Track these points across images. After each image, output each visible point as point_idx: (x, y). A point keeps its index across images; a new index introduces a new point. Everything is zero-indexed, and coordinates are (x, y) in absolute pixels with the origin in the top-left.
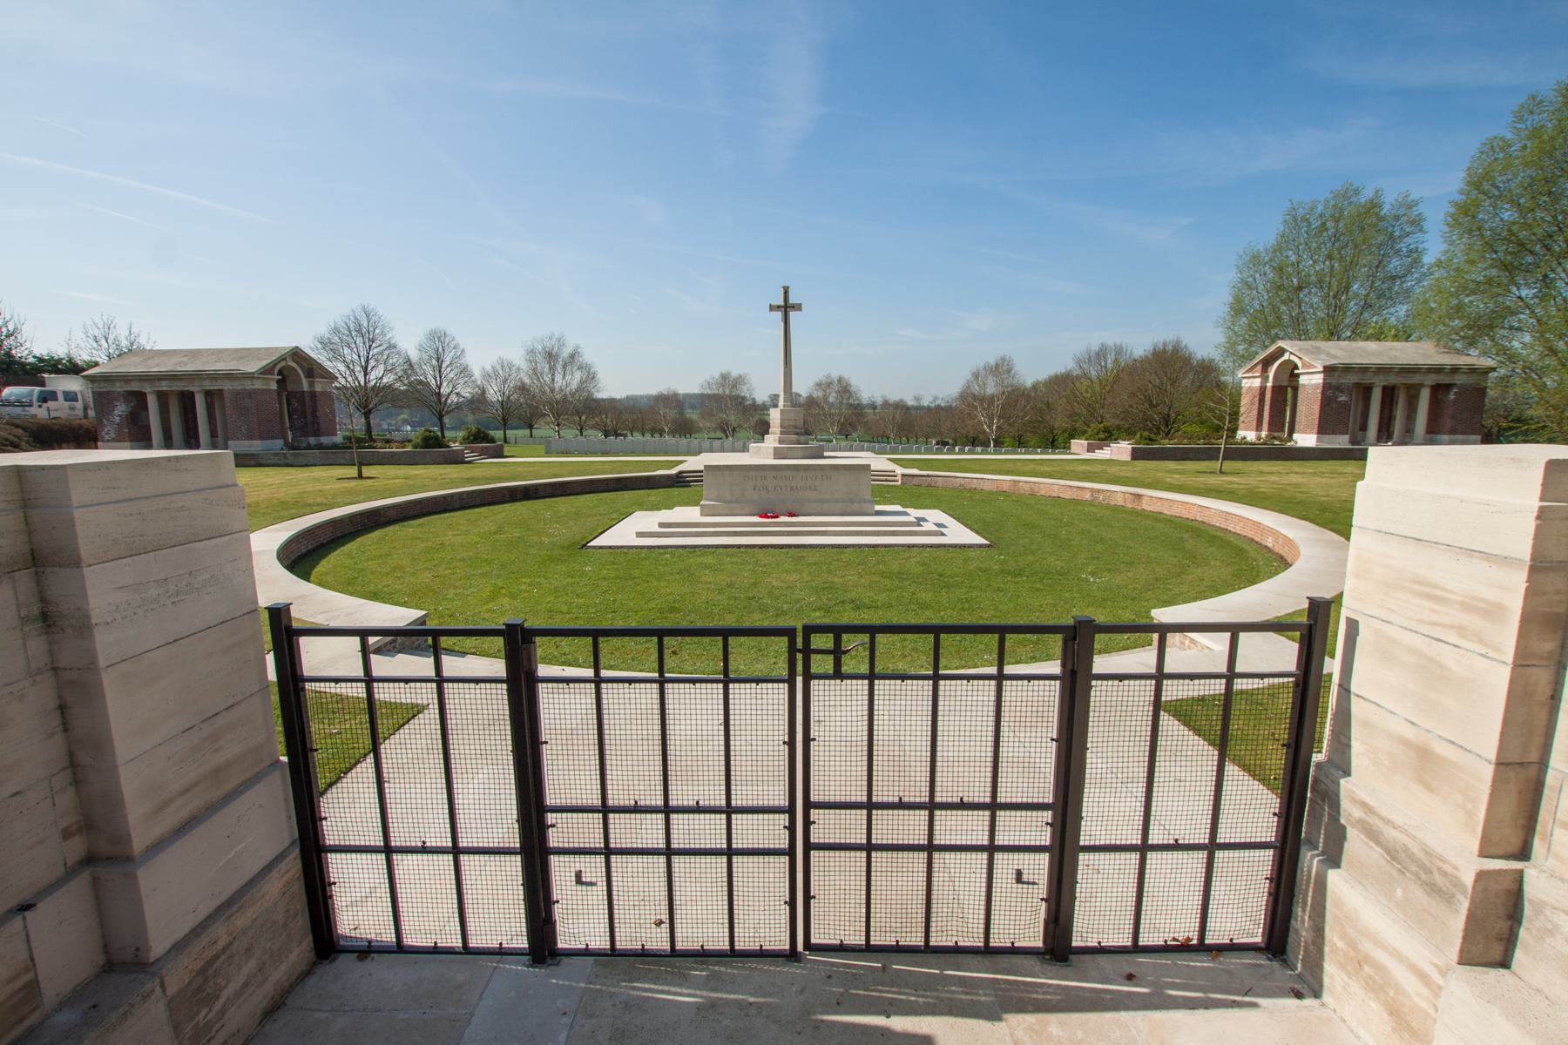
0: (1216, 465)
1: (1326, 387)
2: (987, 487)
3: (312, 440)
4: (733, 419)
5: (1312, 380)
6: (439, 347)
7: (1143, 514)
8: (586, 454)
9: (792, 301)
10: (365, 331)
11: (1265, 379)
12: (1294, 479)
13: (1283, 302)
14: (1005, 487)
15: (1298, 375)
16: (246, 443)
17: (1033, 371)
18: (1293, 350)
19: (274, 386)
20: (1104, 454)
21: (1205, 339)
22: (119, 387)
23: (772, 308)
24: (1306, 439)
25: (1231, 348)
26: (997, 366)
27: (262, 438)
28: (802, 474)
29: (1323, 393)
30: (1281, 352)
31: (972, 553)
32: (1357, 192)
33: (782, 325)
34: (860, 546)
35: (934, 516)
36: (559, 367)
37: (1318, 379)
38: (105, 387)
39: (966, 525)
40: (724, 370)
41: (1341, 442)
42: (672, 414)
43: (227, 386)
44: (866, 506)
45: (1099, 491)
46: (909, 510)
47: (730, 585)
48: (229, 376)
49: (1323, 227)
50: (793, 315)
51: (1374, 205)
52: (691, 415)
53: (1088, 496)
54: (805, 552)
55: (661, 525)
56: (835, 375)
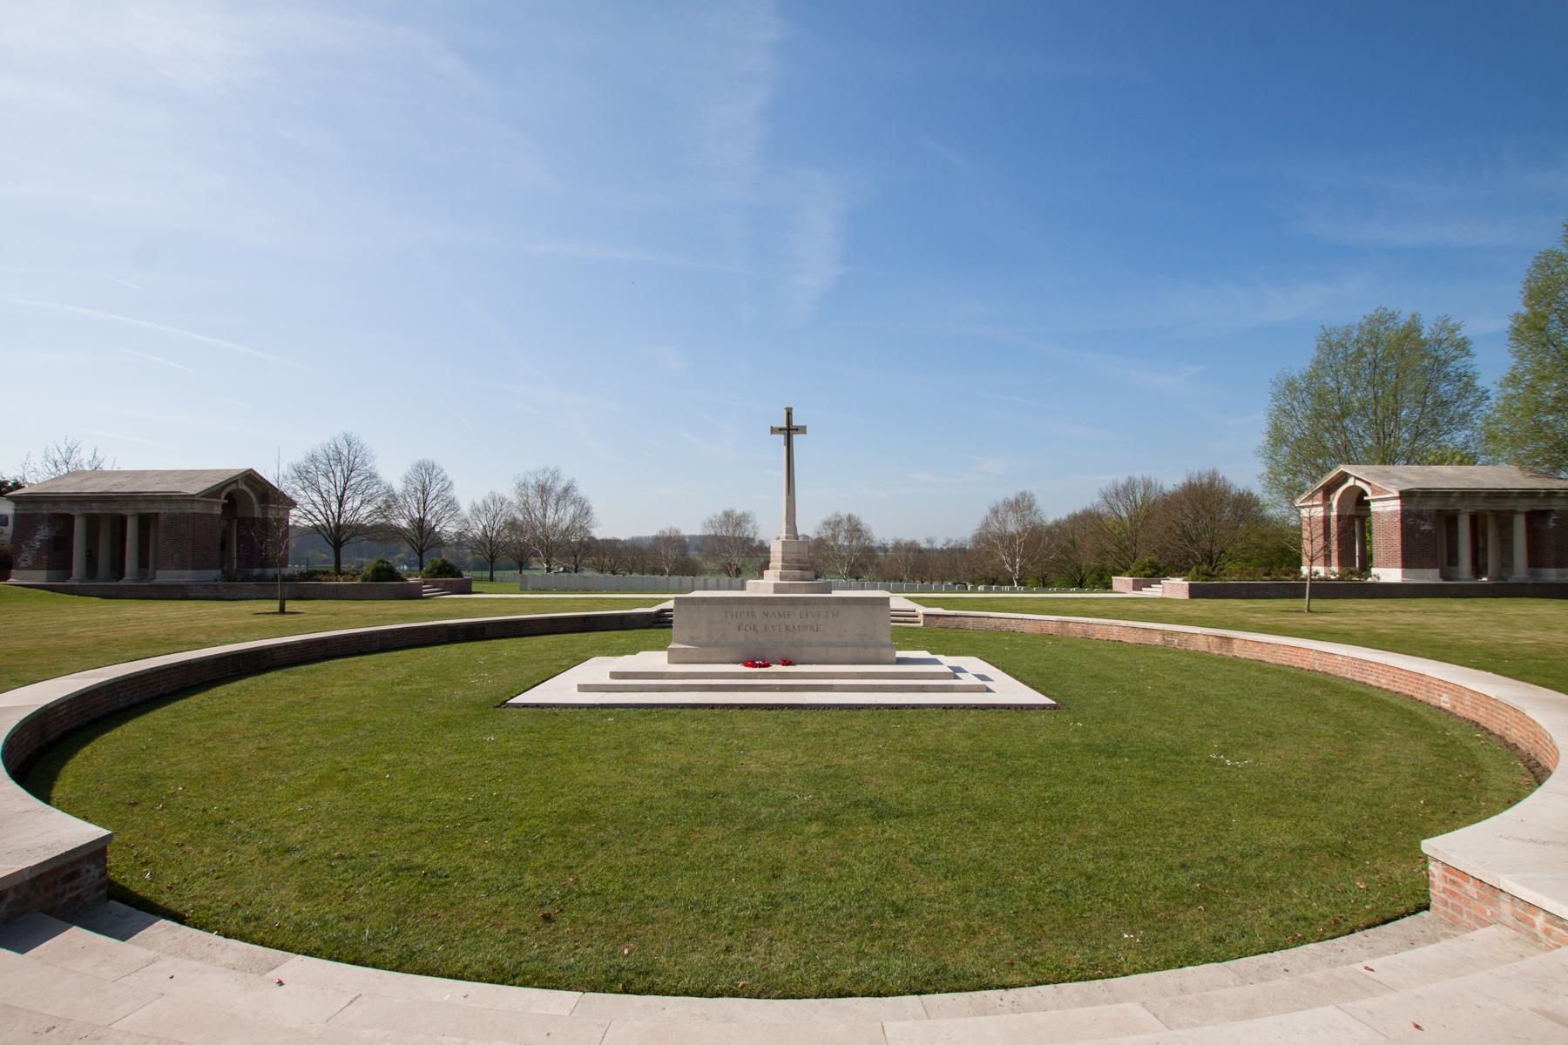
0: (1303, 604)
1: (1405, 515)
2: (1028, 628)
3: (256, 571)
4: (737, 560)
5: (1385, 508)
6: (425, 480)
7: (1235, 661)
8: (565, 591)
9: (795, 423)
10: (345, 464)
11: (1328, 507)
12: (1408, 618)
13: (1327, 430)
14: (1051, 629)
15: (1368, 503)
16: (177, 572)
17: (1055, 508)
18: (1359, 475)
19: (218, 511)
20: (1155, 591)
21: (1246, 472)
22: (46, 509)
23: (773, 430)
24: (1390, 574)
25: (1273, 480)
26: (1017, 501)
27: (193, 568)
28: (800, 609)
29: (1402, 521)
30: (1344, 477)
31: (1037, 719)
32: (1392, 317)
33: (785, 448)
34: (878, 707)
35: (973, 666)
36: (552, 502)
37: (1395, 506)
38: (30, 509)
39: (1016, 678)
40: (728, 508)
41: (1430, 576)
42: (673, 554)
43: (163, 509)
44: (885, 652)
45: (1172, 633)
46: (940, 658)
47: (685, 770)
48: (167, 498)
49: (1361, 353)
50: (796, 438)
51: (1412, 330)
52: (693, 554)
53: (1158, 640)
54: (802, 716)
55: (614, 675)
56: (844, 514)
